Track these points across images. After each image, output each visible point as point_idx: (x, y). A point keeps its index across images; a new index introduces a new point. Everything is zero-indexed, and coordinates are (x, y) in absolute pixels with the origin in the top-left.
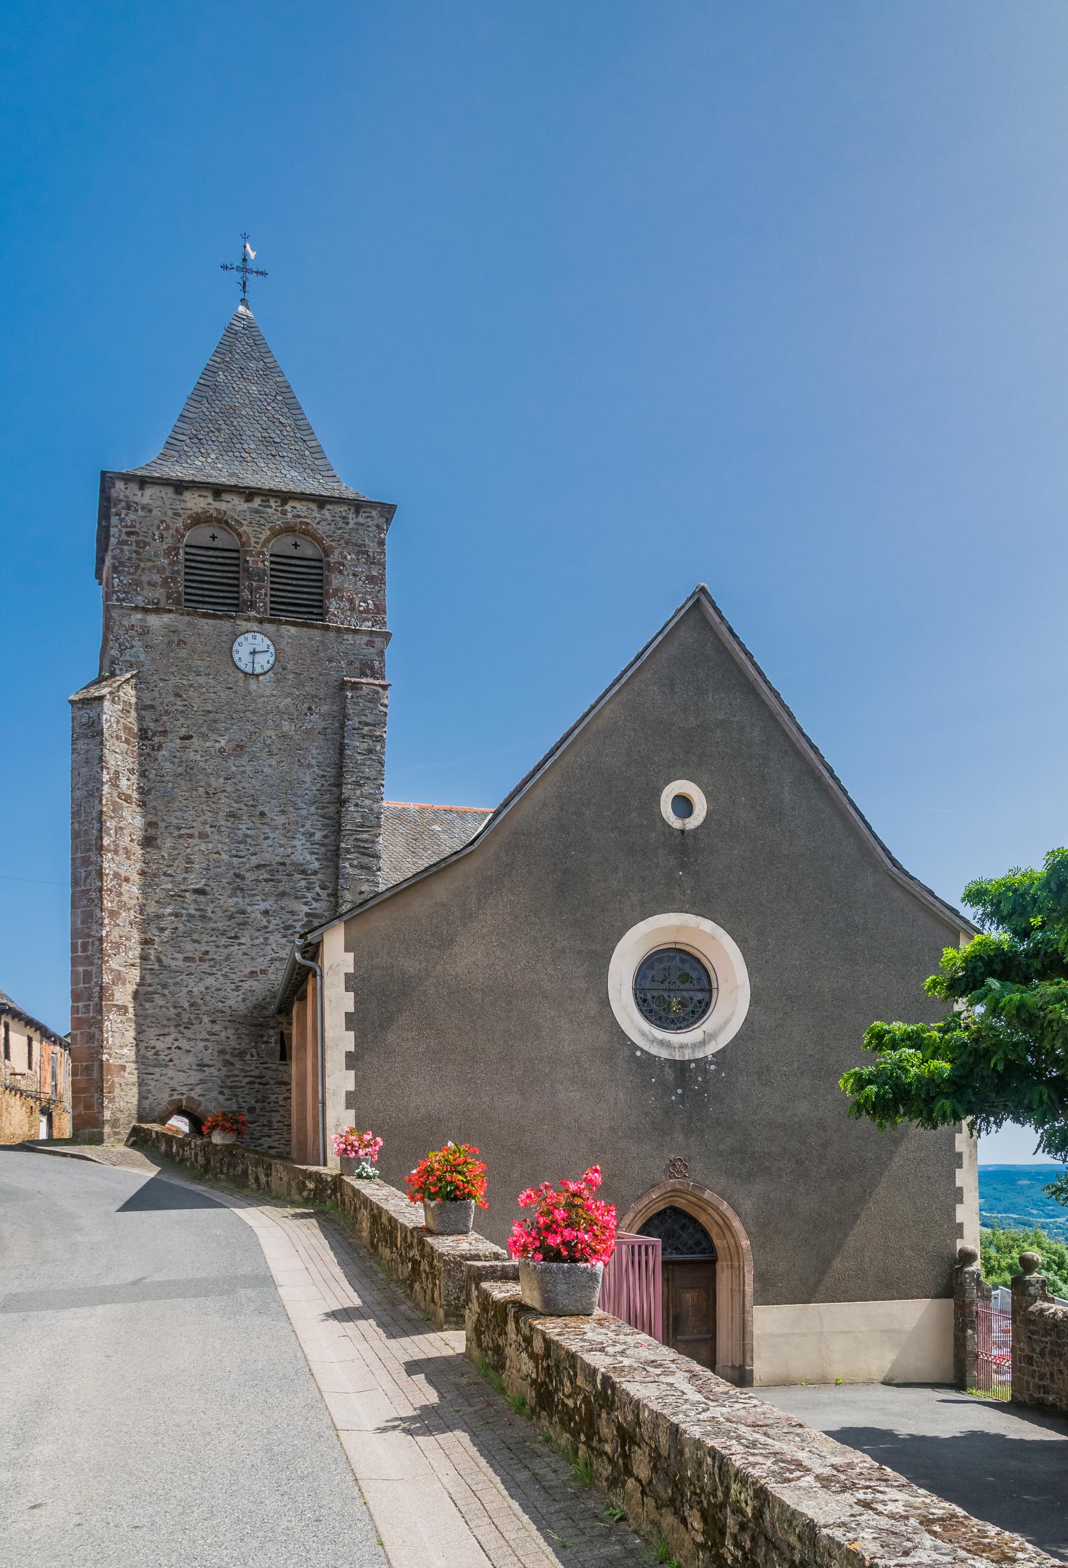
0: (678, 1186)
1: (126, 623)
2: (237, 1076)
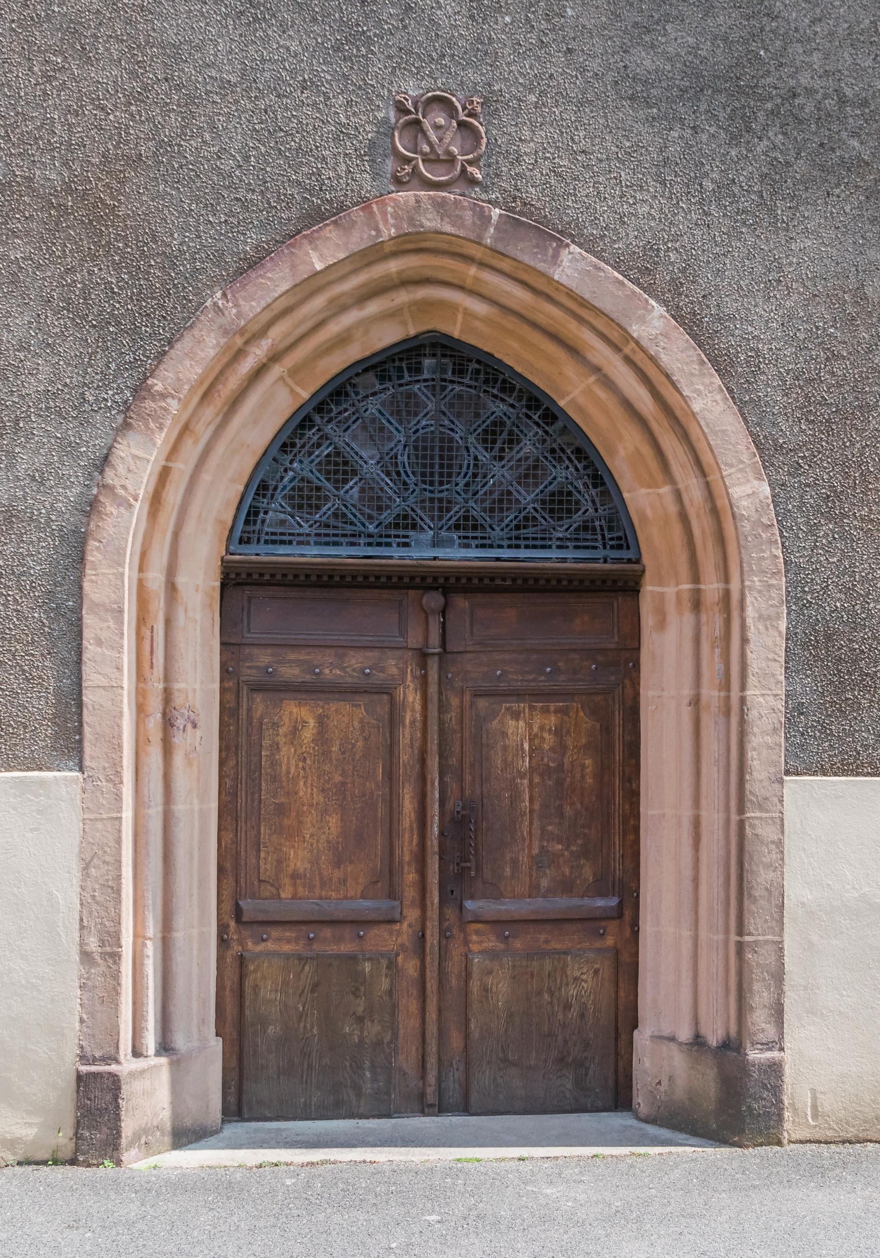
0: (430, 221)
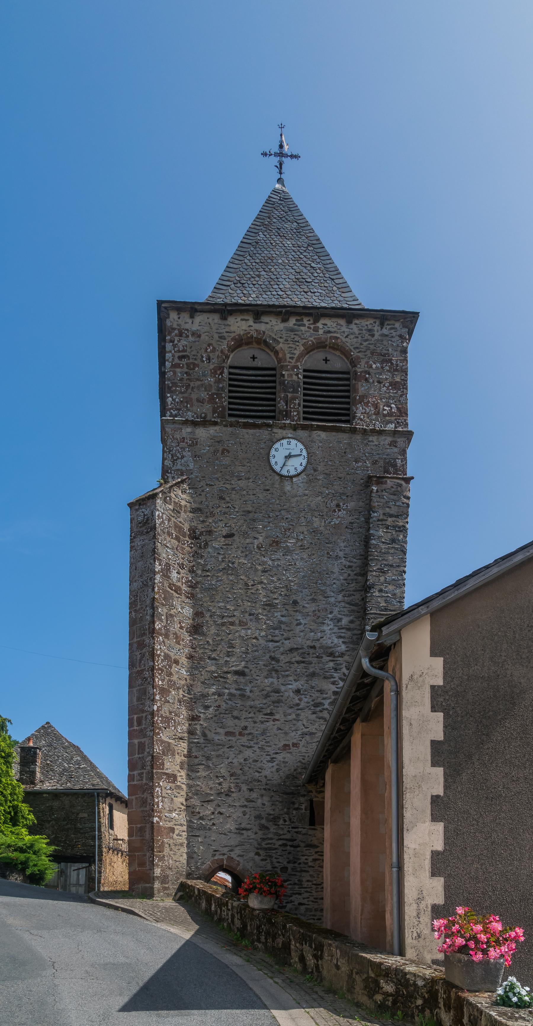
1: (178, 436)
2: (271, 839)
